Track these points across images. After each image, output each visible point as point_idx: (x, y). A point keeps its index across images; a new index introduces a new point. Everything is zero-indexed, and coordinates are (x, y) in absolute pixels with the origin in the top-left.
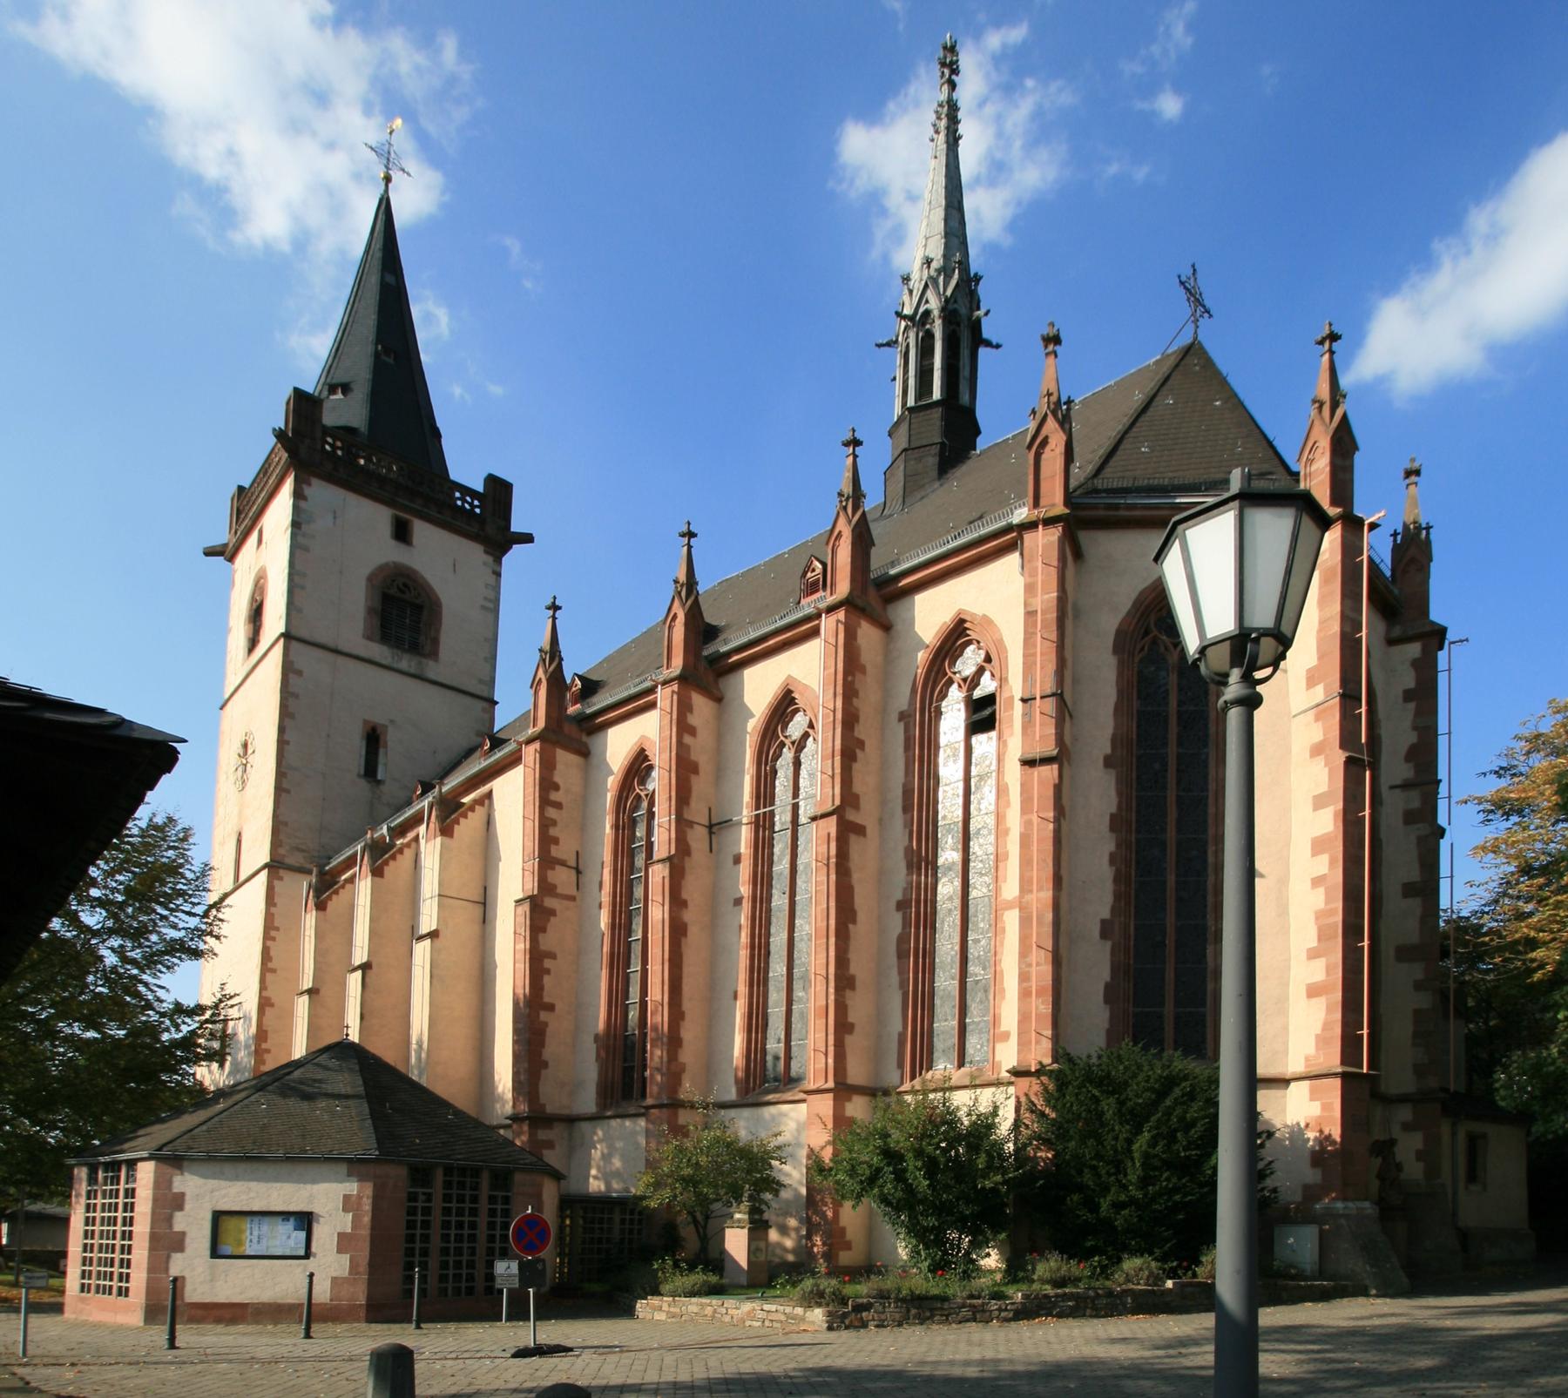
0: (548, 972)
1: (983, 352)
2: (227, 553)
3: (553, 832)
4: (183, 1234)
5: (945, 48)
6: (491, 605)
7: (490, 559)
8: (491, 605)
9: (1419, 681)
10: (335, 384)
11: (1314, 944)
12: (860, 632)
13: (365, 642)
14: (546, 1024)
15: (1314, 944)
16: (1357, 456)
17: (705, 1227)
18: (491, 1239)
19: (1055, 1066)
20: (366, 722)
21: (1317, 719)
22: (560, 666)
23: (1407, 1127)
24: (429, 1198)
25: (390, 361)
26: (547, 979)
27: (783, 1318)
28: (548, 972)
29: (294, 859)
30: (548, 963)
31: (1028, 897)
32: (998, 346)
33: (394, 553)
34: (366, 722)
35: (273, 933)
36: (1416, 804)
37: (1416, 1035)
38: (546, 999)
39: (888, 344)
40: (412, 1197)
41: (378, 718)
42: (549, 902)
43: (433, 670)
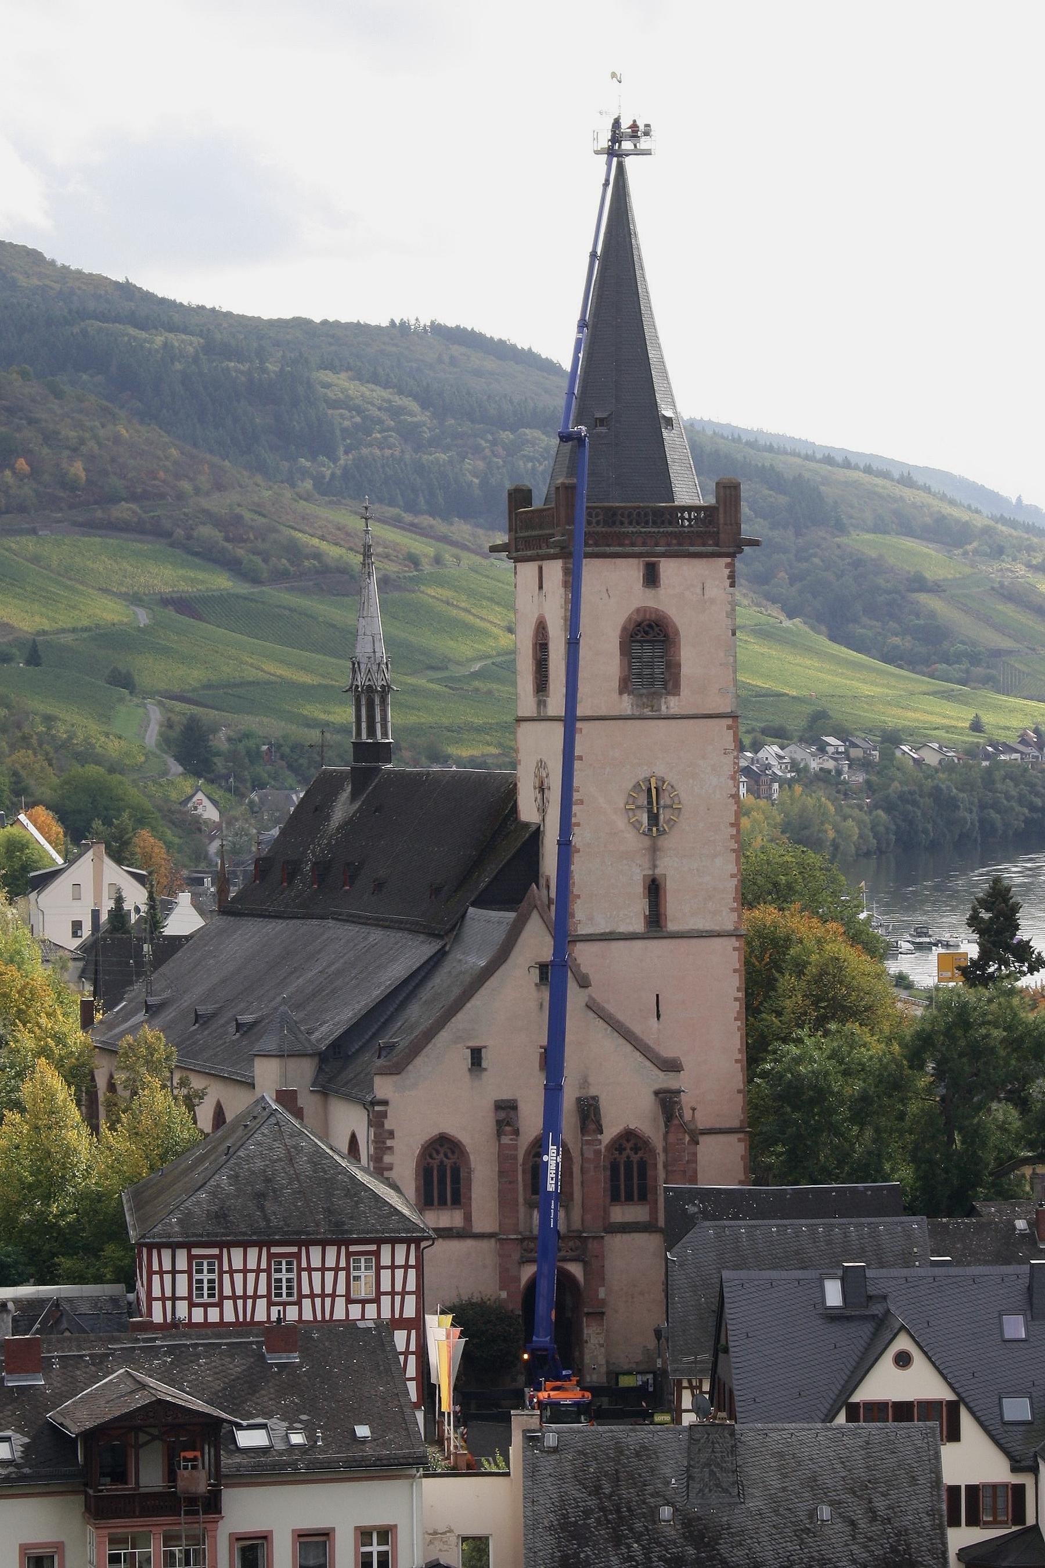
43: (672, 704)
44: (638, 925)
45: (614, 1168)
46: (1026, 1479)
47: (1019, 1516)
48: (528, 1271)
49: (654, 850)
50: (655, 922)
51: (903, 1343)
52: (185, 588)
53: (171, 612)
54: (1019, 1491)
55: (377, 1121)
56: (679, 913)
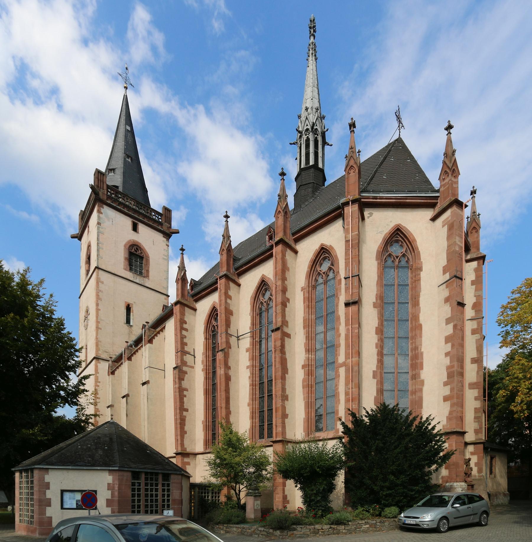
0: (185, 396)
1: (326, 147)
2: (79, 237)
3: (185, 340)
4: (50, 499)
5: (311, 21)
6: (166, 258)
7: (165, 239)
8: (166, 258)
9: (477, 277)
10: (110, 170)
11: (446, 380)
12: (287, 253)
13: (124, 271)
14: (185, 417)
15: (446, 380)
16: (460, 177)
17: (239, 495)
18: (164, 501)
19: (366, 420)
20: (126, 302)
21: (447, 287)
22: (185, 274)
23: (472, 454)
24: (139, 484)
25: (130, 160)
26: (185, 399)
27: (266, 533)
28: (185, 396)
29: (104, 356)
30: (185, 393)
31: (348, 361)
32: (331, 145)
33: (133, 236)
34: (126, 302)
35: (98, 384)
36: (475, 326)
37: (475, 418)
38: (185, 407)
39: (294, 144)
40: (133, 484)
41: (130, 302)
42: (185, 368)
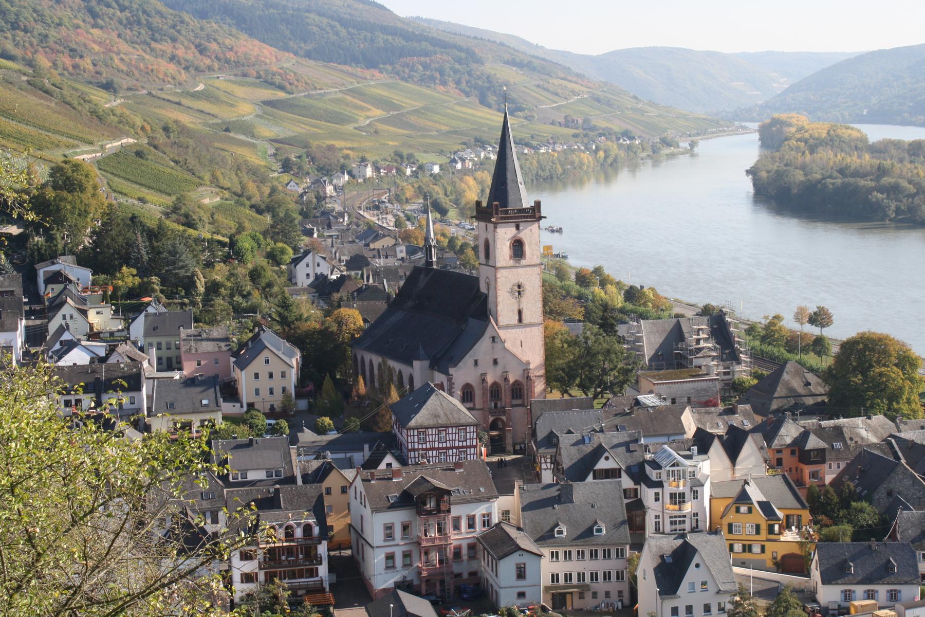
43: (523, 262)
44: (516, 322)
45: (513, 390)
46: (638, 487)
47: (636, 496)
48: (491, 419)
49: (519, 302)
50: (520, 320)
51: (606, 454)
52: (272, 98)
53: (269, 109)
54: (636, 490)
55: (450, 380)
56: (526, 319)
